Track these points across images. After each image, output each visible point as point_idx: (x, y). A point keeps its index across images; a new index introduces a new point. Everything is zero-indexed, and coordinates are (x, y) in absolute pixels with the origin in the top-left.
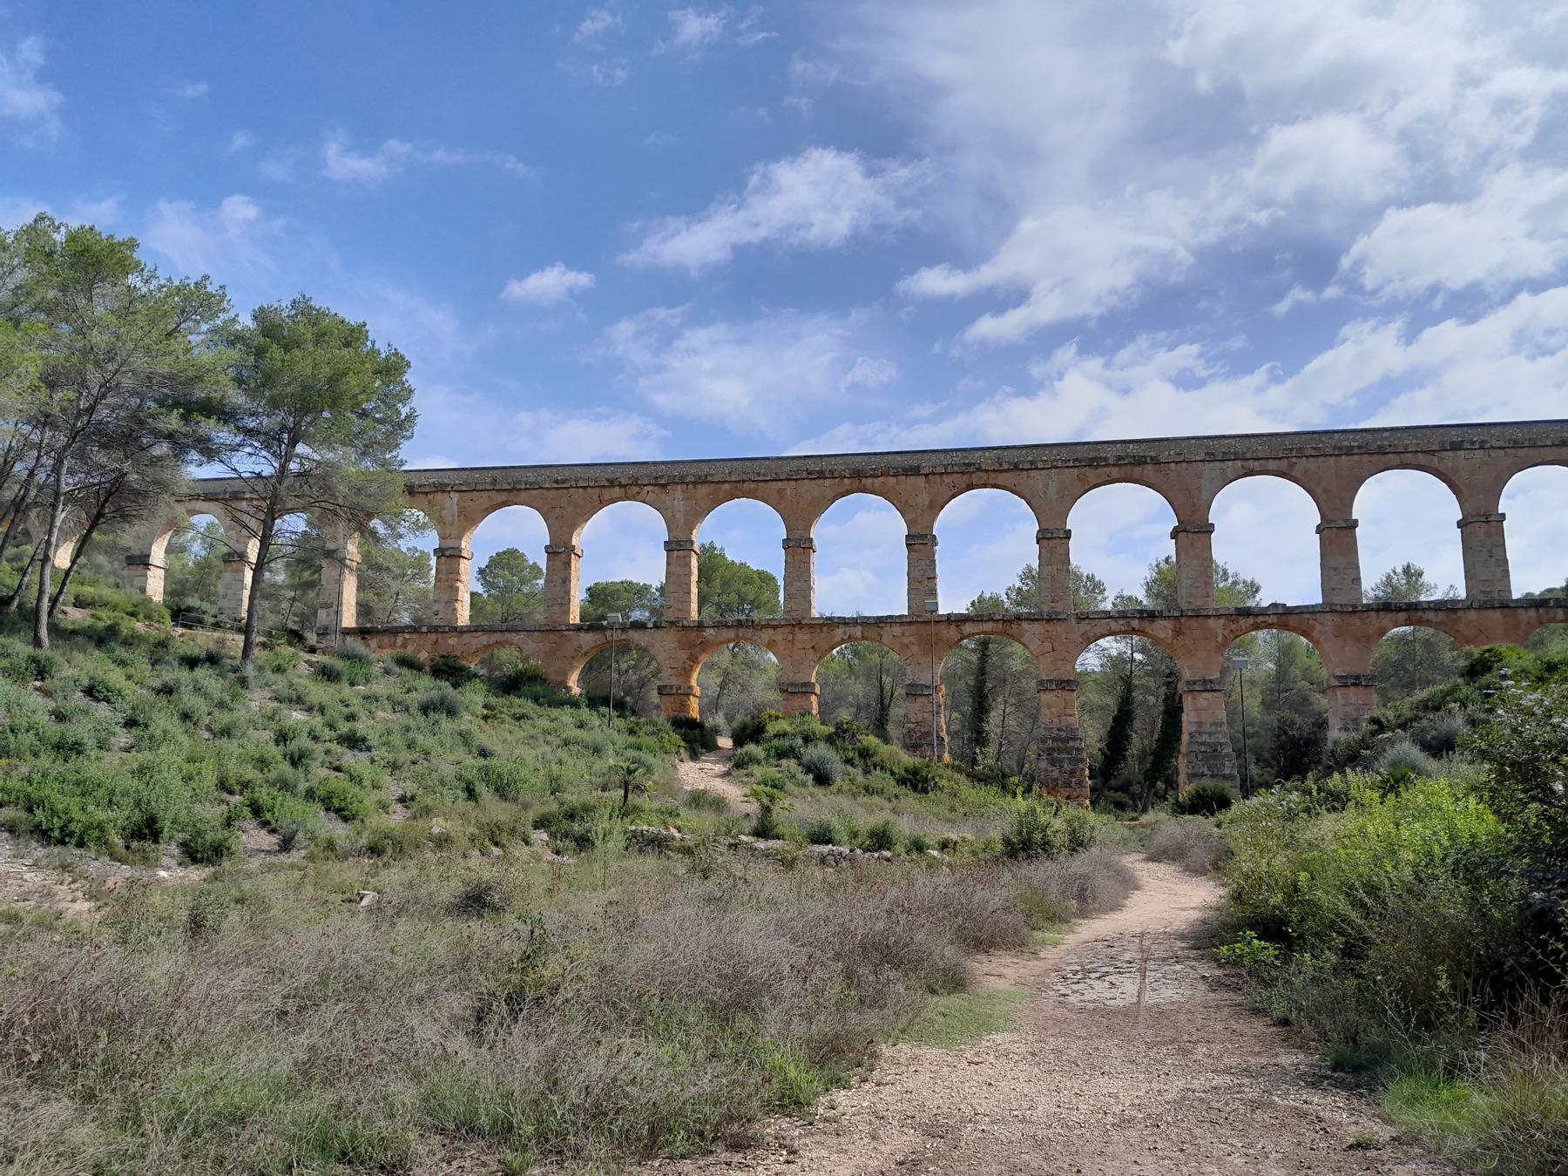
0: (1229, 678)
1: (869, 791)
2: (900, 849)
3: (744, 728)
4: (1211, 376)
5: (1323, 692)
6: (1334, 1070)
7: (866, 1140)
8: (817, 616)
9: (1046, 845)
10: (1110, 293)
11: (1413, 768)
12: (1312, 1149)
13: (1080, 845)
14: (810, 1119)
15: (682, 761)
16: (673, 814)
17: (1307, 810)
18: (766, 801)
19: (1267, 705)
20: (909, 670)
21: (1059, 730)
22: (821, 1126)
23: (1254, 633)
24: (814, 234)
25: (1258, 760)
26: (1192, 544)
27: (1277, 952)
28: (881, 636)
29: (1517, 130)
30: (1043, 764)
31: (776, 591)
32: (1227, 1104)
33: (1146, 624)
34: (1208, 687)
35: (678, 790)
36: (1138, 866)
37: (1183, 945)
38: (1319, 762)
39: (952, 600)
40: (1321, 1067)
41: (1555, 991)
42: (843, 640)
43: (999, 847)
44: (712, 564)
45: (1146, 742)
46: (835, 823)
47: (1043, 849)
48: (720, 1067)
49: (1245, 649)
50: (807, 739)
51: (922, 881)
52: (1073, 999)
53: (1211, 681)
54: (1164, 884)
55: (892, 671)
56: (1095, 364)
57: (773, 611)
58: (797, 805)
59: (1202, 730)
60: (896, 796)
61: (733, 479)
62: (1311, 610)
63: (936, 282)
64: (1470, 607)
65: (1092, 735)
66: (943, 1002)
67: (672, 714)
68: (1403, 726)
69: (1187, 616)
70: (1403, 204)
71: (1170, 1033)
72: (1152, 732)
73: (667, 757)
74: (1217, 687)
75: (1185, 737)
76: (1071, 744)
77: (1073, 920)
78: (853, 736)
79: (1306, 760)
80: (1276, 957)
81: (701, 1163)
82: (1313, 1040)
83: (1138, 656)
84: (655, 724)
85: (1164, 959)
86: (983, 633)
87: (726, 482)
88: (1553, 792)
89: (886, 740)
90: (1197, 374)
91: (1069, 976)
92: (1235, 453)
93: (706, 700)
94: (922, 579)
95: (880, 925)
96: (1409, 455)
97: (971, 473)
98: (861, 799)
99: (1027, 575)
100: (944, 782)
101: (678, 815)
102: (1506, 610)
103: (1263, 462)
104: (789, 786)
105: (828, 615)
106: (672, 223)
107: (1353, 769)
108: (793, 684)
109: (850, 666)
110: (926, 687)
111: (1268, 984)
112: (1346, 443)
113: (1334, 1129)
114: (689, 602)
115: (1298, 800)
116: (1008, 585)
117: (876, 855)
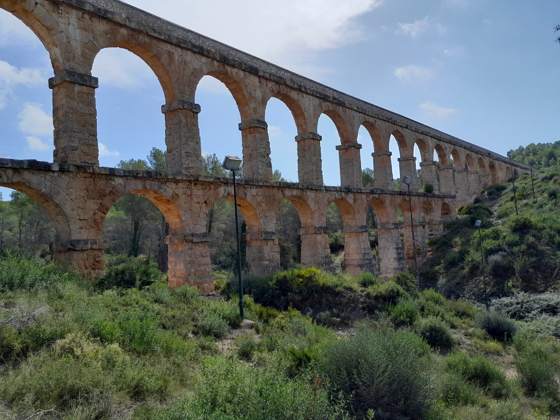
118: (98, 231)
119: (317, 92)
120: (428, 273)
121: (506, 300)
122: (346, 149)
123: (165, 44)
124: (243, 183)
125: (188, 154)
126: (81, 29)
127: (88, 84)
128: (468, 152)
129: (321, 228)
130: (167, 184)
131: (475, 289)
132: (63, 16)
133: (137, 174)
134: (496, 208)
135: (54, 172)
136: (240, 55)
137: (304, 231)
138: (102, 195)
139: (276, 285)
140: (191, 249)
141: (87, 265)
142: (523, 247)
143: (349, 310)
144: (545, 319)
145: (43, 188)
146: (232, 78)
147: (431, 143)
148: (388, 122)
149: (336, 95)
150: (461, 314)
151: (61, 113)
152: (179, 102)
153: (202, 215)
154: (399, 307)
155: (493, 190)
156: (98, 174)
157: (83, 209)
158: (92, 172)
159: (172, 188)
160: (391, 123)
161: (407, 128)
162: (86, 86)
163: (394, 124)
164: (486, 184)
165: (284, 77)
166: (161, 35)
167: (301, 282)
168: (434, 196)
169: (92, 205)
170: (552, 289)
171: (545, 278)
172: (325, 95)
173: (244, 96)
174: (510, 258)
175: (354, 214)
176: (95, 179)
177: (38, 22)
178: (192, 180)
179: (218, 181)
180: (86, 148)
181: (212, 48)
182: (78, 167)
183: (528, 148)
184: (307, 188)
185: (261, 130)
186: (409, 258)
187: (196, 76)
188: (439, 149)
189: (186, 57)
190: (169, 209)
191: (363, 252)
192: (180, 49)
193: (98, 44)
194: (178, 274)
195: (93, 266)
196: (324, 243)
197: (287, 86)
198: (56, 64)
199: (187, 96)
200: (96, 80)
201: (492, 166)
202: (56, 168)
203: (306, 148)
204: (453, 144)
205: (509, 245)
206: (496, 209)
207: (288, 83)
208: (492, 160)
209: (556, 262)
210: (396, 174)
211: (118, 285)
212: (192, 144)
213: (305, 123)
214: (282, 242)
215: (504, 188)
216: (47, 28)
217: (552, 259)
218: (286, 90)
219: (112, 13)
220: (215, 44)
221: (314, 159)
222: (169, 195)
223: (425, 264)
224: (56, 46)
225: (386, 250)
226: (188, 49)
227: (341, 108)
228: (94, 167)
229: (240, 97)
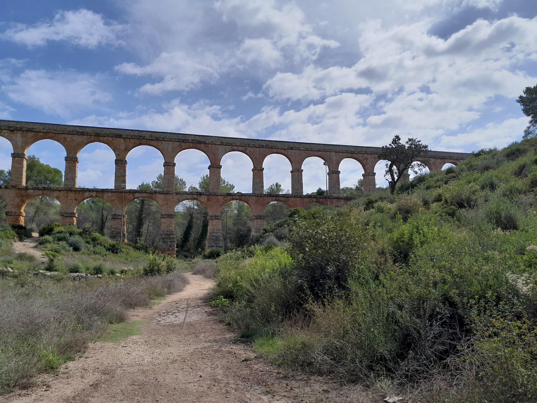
0: (223, 215)
1: (95, 253)
2: (105, 274)
3: (44, 229)
4: (223, 117)
5: (251, 220)
6: (241, 338)
7: (79, 379)
8: (78, 187)
9: (159, 271)
10: (191, 83)
11: (274, 244)
12: (231, 363)
13: (170, 270)
14: (57, 373)
15: (15, 241)
16: (10, 262)
17: (243, 257)
18: (51, 257)
19: (234, 224)
20: (113, 209)
21: (167, 231)
22: (61, 376)
23: (232, 201)
24: (83, 42)
25: (230, 241)
26: (215, 171)
27: (229, 302)
28: (103, 196)
29: (313, 55)
30: (161, 243)
31: (61, 177)
32: (208, 352)
33: (199, 197)
34: (217, 218)
35: (13, 253)
36: (189, 276)
37: (201, 301)
38: (248, 242)
39: (131, 185)
40: (237, 337)
41: (301, 309)
42: (88, 197)
43: (142, 272)
44: (33, 165)
45: (196, 236)
46: (80, 265)
47: (158, 272)
48: (19, 358)
49: (229, 206)
50: (71, 234)
51: (112, 284)
52: (162, 322)
53: (218, 216)
54: (197, 282)
55: (107, 210)
56: (186, 107)
57: (60, 184)
58: (65, 259)
59: (214, 231)
60: (105, 255)
61: (45, 131)
62: (249, 195)
63: (129, 68)
64: (292, 197)
65: (179, 233)
66: (115, 326)
67: (12, 223)
68: (272, 231)
69: (212, 195)
70: (282, 71)
71: (193, 331)
72: (198, 232)
73: (9, 240)
74: (219, 218)
75: (208, 234)
76: (171, 236)
77: (166, 296)
78: (90, 233)
79: (244, 241)
80: (229, 304)
81: (7, 396)
82: (236, 329)
83: (196, 207)
84: (3, 227)
85: (194, 307)
86: (143, 197)
87: (42, 132)
88: (306, 251)
89: (103, 235)
90: (218, 116)
91: (162, 314)
92: (229, 143)
93: (28, 218)
94: (120, 176)
95: (93, 301)
96: (279, 150)
97: (141, 139)
98: (92, 256)
99: (160, 177)
100: (124, 250)
101: (12, 263)
102: (301, 198)
103: (237, 147)
104: (62, 251)
105: (82, 187)
106: (20, 26)
107: (257, 244)
108: (66, 213)
109: (91, 207)
110: (120, 215)
111: (225, 312)
112: (262, 144)
113: (239, 356)
114: (21, 179)
115: (240, 254)
116: (152, 181)
117: (96, 276)
169: (18, 200)
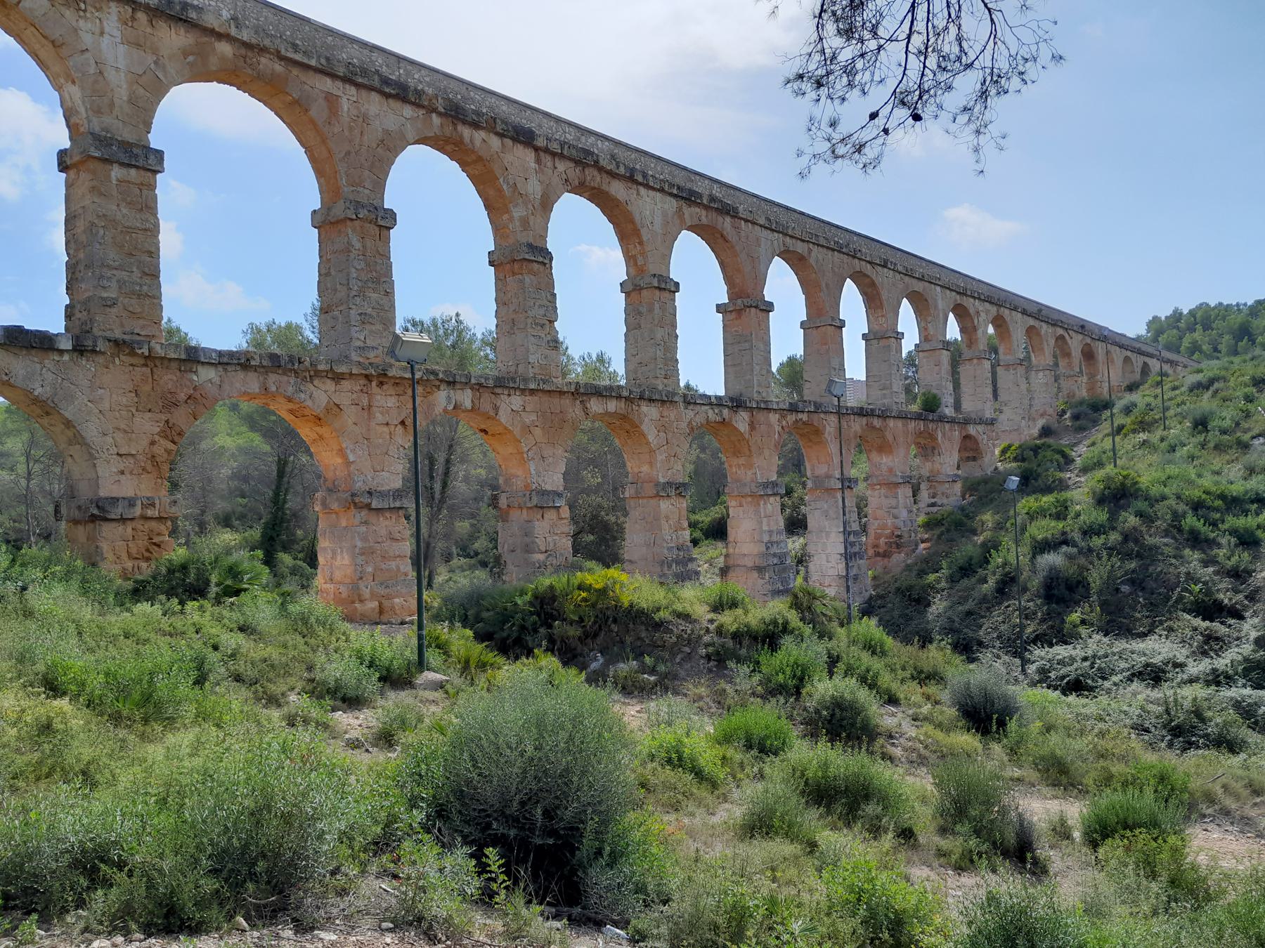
118: (159, 480)
119: (672, 185)
120: (910, 588)
121: (1061, 651)
122: (739, 312)
123: (319, 76)
124: (491, 383)
125: (365, 319)
126: (129, 43)
127: (141, 163)
128: (1031, 322)
129: (669, 484)
130: (316, 382)
131: (1003, 628)
132: (88, 15)
133: (248, 360)
134: (1082, 449)
135: (61, 352)
136: (493, 100)
137: (633, 491)
138: (170, 404)
139: (531, 604)
140: (366, 523)
141: (134, 551)
142: (1114, 537)
143: (678, 660)
144: (1134, 694)
145: (37, 385)
146: (473, 152)
147: (942, 299)
148: (839, 252)
149: (716, 191)
150: (925, 677)
151: (81, 225)
152: (348, 204)
153: (393, 451)
154: (780, 655)
155: (1084, 408)
156: (162, 358)
157: (125, 431)
158: (147, 354)
159: (325, 392)
160: (848, 255)
161: (885, 266)
162: (135, 166)
163: (854, 257)
164: (1071, 395)
165: (596, 151)
166: (310, 57)
167: (585, 600)
168: (942, 419)
169: (148, 425)
170: (1164, 630)
171: (1152, 606)
172: (690, 190)
173: (500, 190)
174: (1082, 561)
175: (750, 456)
176: (155, 370)
177: (33, 29)
178: (371, 375)
179: (432, 377)
180: (133, 301)
181: (429, 85)
182: (116, 343)
183: (1192, 313)
184: (641, 398)
185: (536, 266)
186: (877, 554)
187: (391, 147)
188: (962, 313)
189: (366, 106)
190: (321, 438)
191: (766, 538)
192: (353, 88)
193: (166, 77)
194: (338, 575)
195: (147, 554)
196: (676, 517)
197: (601, 169)
198: (73, 120)
199: (367, 192)
200: (159, 155)
201: (1089, 355)
202: (66, 344)
203: (644, 310)
204: (996, 305)
205: (1085, 533)
206: (1082, 453)
207: (604, 163)
208: (1088, 340)
209: (1179, 573)
210: (855, 365)
211: (170, 593)
212: (374, 295)
213: (643, 254)
214: (603, 513)
215: (1108, 405)
216: (53, 42)
217: (1171, 564)
218: (598, 179)
219: (199, 9)
220: (436, 76)
221: (660, 333)
222: (318, 406)
223: (908, 568)
224: (73, 82)
225: (824, 535)
226: (371, 89)
227: (728, 219)
228: (153, 343)
229: (491, 192)
